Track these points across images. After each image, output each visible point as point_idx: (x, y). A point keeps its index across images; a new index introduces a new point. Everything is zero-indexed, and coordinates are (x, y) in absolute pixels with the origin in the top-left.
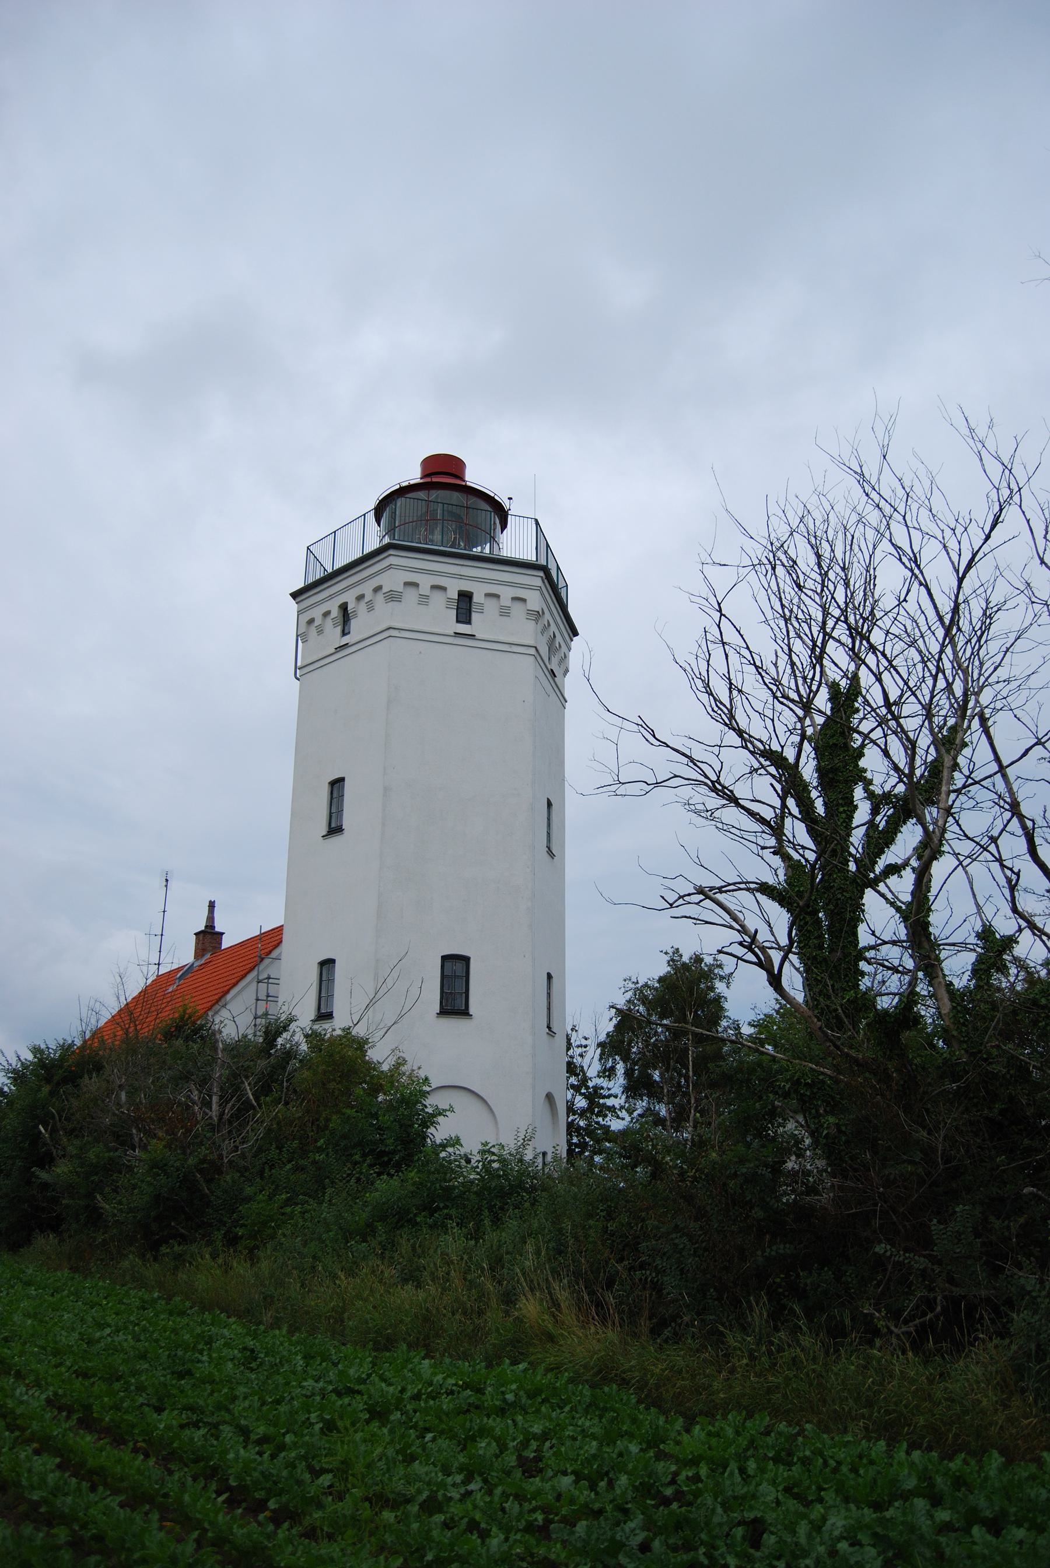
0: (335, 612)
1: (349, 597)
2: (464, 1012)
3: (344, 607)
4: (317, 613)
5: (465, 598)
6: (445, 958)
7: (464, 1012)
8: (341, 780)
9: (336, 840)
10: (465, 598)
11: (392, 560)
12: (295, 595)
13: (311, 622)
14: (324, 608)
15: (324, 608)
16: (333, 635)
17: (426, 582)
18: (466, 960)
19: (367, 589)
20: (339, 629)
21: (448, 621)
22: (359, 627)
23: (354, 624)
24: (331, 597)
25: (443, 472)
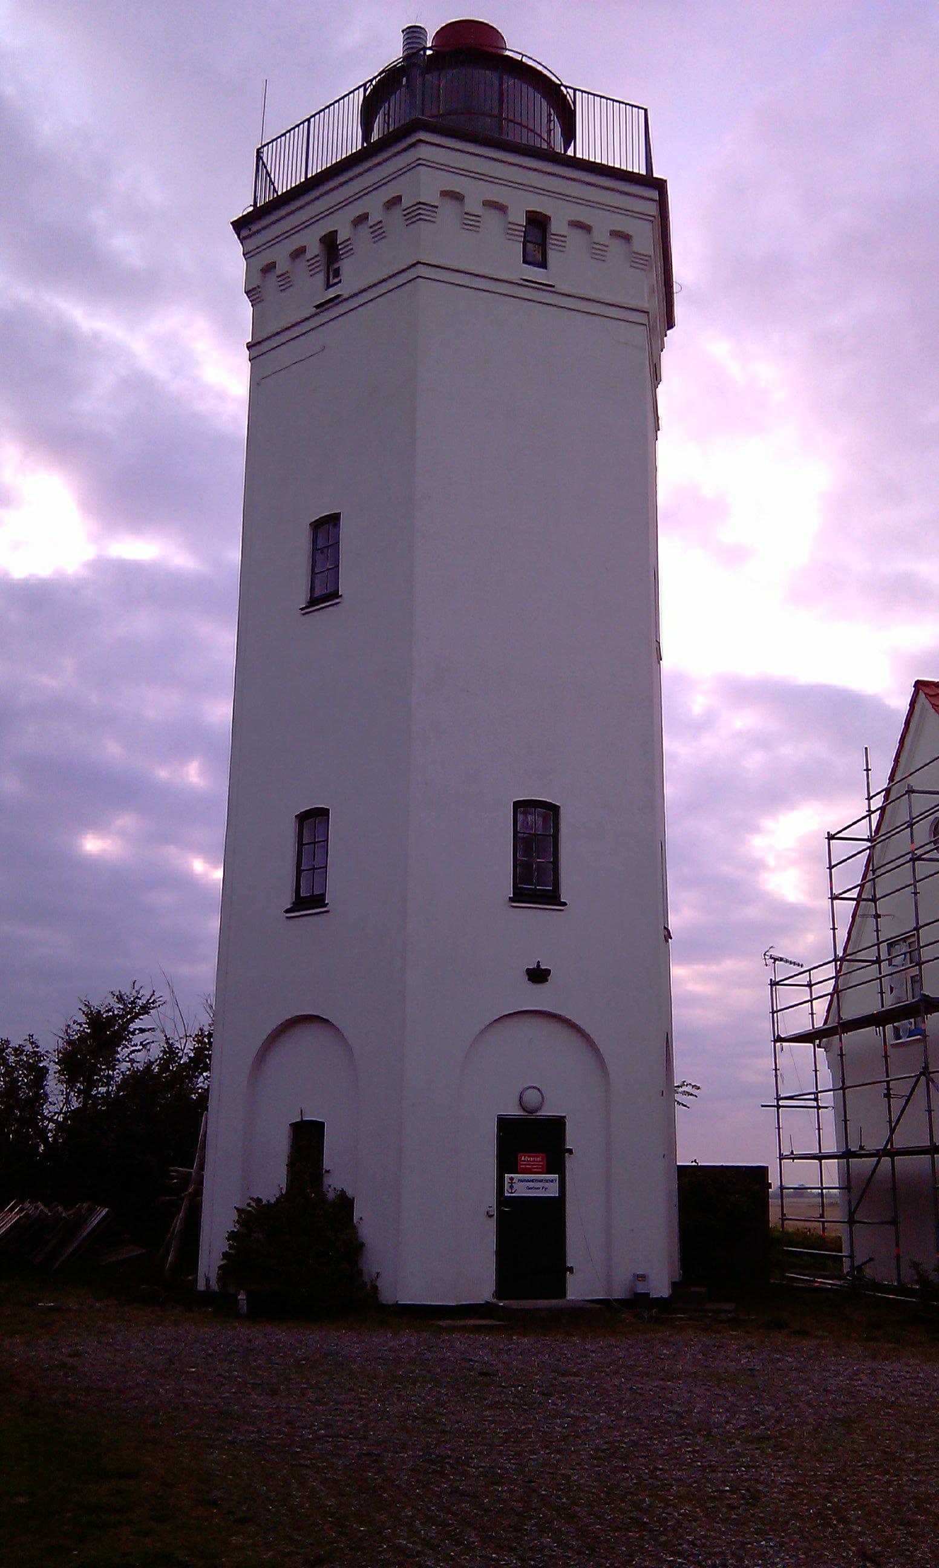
0: (314, 249)
1: (341, 224)
2: (552, 898)
3: (330, 243)
4: (280, 255)
5: (538, 223)
6: (517, 805)
7: (552, 898)
8: (322, 814)
9: (327, 616)
10: (538, 223)
11: (423, 151)
12: (240, 225)
13: (269, 268)
14: (356, 210)
15: (294, 243)
16: (310, 287)
17: (475, 193)
18: (551, 811)
19: (373, 205)
20: (320, 278)
21: (506, 257)
22: (354, 273)
23: (346, 265)
24: (306, 225)
25: (469, 47)
